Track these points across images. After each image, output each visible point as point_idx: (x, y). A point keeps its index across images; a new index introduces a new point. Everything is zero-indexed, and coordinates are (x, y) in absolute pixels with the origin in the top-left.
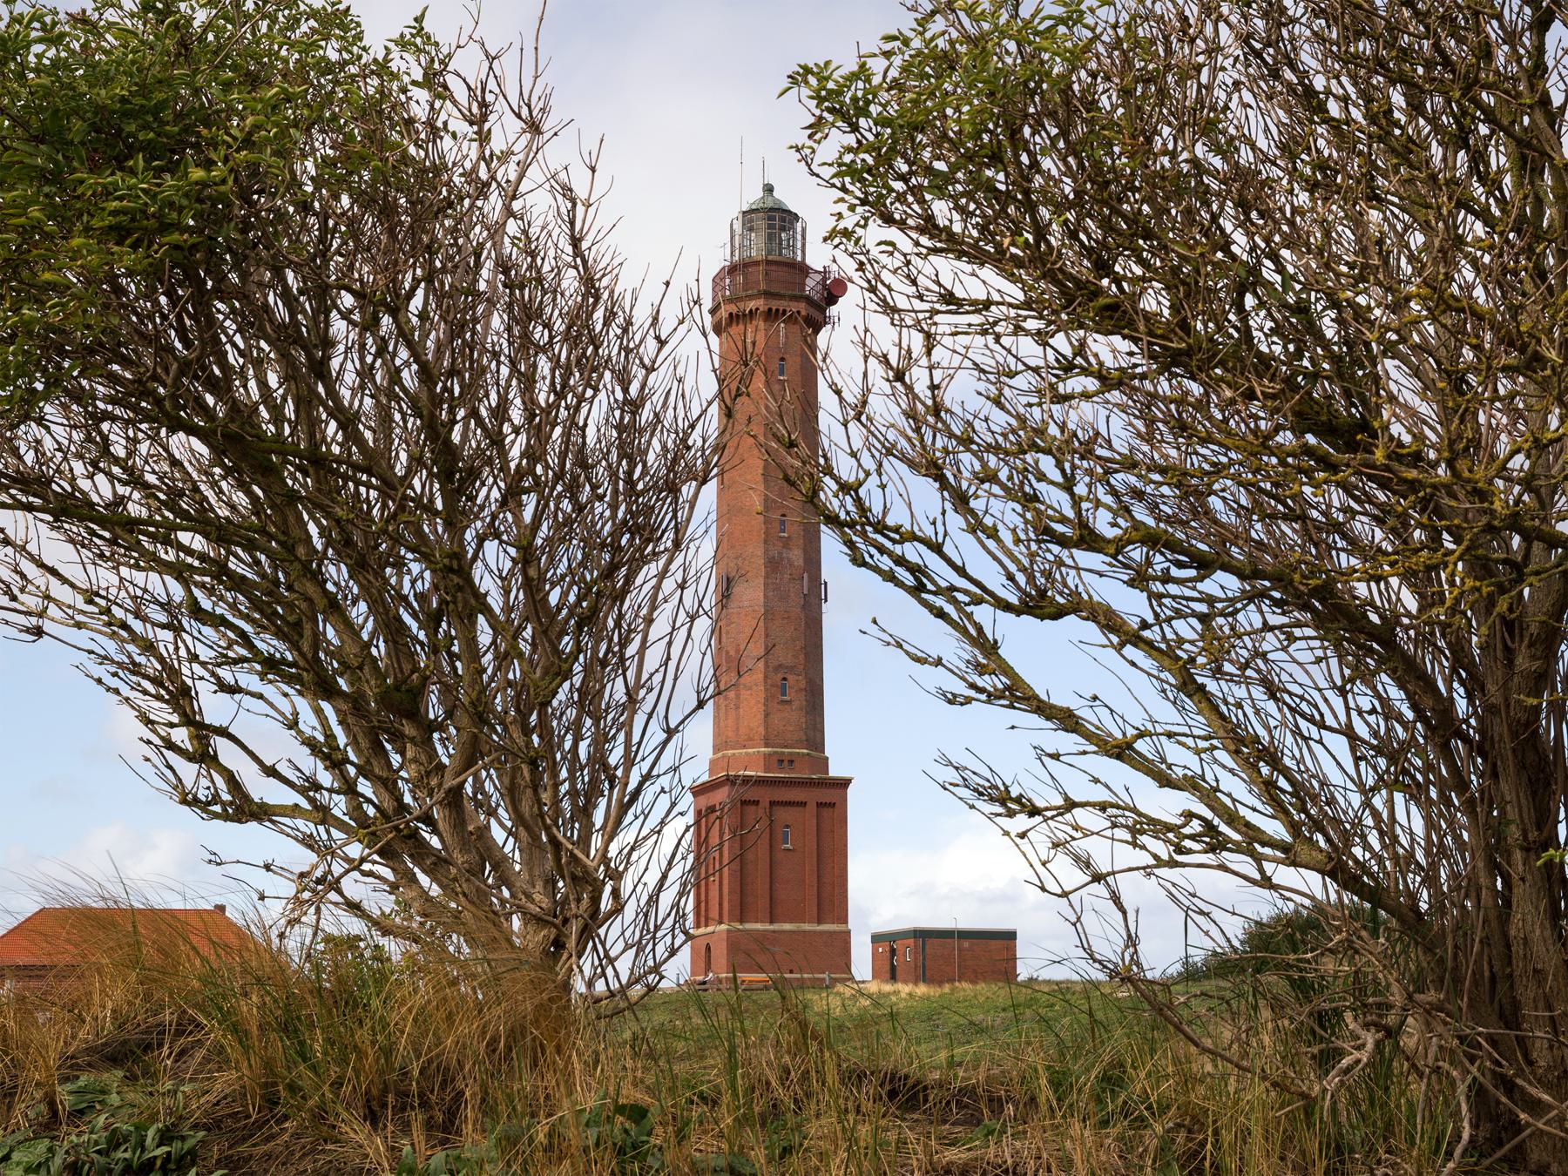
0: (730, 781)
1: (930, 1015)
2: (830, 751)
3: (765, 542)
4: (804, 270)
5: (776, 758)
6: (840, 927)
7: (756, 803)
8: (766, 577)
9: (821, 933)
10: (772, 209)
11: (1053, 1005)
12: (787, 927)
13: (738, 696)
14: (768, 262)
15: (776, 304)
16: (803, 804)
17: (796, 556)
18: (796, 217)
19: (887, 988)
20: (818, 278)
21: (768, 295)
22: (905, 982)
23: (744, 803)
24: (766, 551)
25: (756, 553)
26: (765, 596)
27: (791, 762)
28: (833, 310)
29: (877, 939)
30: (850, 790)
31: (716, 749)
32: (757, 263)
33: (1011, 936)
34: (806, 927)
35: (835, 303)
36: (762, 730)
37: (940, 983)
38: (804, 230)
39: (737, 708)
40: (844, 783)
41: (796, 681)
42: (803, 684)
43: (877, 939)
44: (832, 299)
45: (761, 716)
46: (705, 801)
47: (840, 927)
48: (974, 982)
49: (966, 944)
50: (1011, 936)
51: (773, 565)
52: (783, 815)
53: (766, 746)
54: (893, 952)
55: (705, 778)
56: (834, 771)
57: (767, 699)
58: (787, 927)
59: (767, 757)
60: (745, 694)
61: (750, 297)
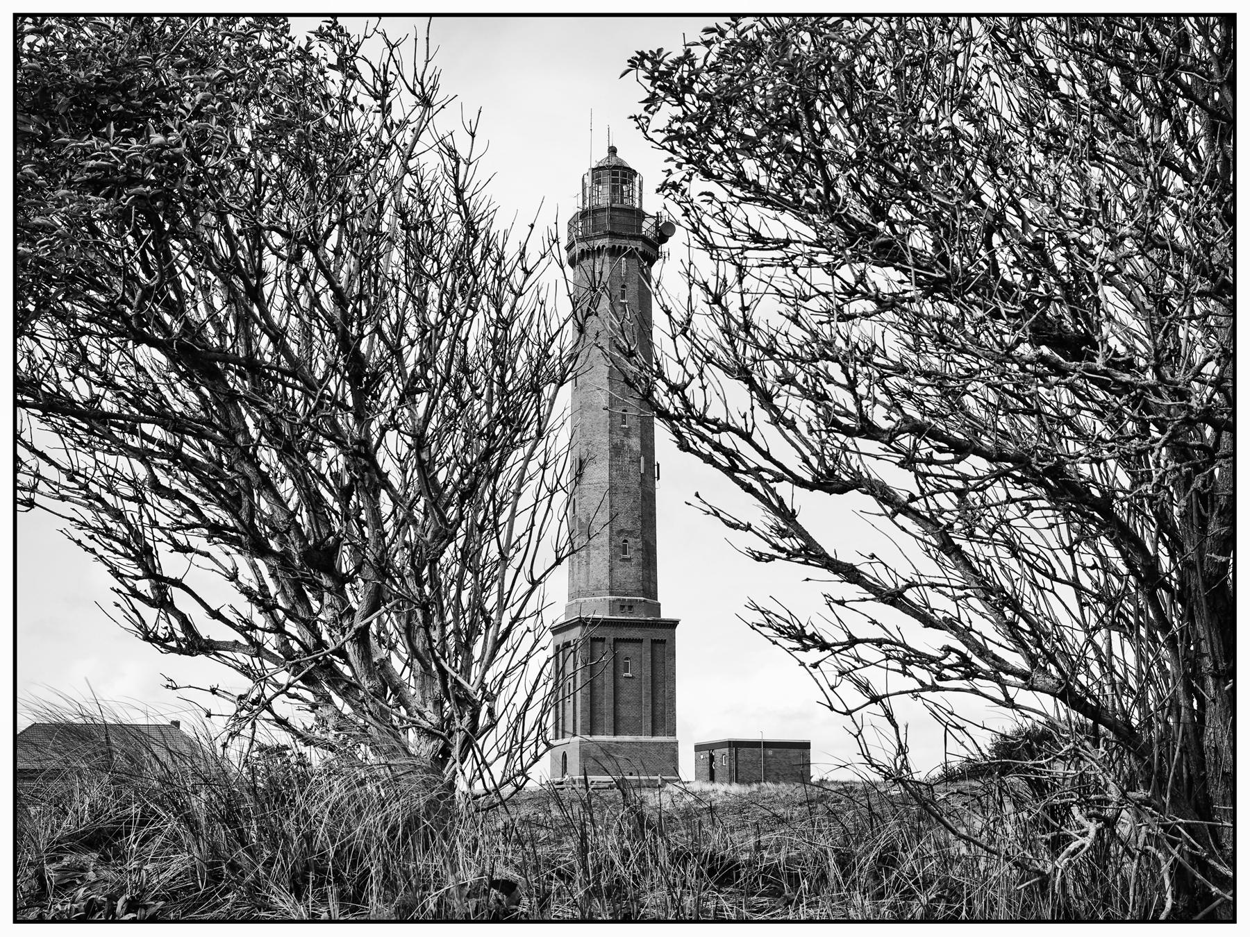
0: (582, 622)
1: (741, 807)
2: (661, 598)
3: (610, 432)
4: (641, 215)
5: (618, 604)
6: (671, 739)
7: (603, 640)
8: (611, 460)
9: (655, 744)
10: (615, 167)
11: (839, 801)
12: (628, 738)
13: (588, 555)
14: (613, 209)
15: (619, 243)
16: (640, 641)
17: (635, 443)
18: (635, 173)
19: (708, 787)
20: (652, 221)
21: (612, 235)
22: (722, 782)
23: (594, 640)
24: (611, 439)
25: (602, 441)
26: (610, 475)
27: (630, 607)
28: (664, 248)
29: (699, 748)
30: (678, 629)
31: (571, 597)
32: (604, 210)
33: (806, 746)
34: (643, 738)
35: (665, 241)
36: (607, 581)
37: (749, 783)
38: (641, 183)
39: (588, 564)
40: (673, 624)
41: (634, 543)
42: (640, 546)
43: (699, 748)
44: (664, 239)
45: (606, 570)
46: (561, 639)
47: (671, 739)
48: (776, 782)
49: (770, 752)
50: (806, 746)
51: (617, 450)
52: (625, 650)
53: (611, 594)
54: (712, 758)
55: (562, 620)
56: (665, 615)
57: (611, 557)
58: (628, 738)
59: (612, 603)
60: (594, 553)
61: (599, 237)
